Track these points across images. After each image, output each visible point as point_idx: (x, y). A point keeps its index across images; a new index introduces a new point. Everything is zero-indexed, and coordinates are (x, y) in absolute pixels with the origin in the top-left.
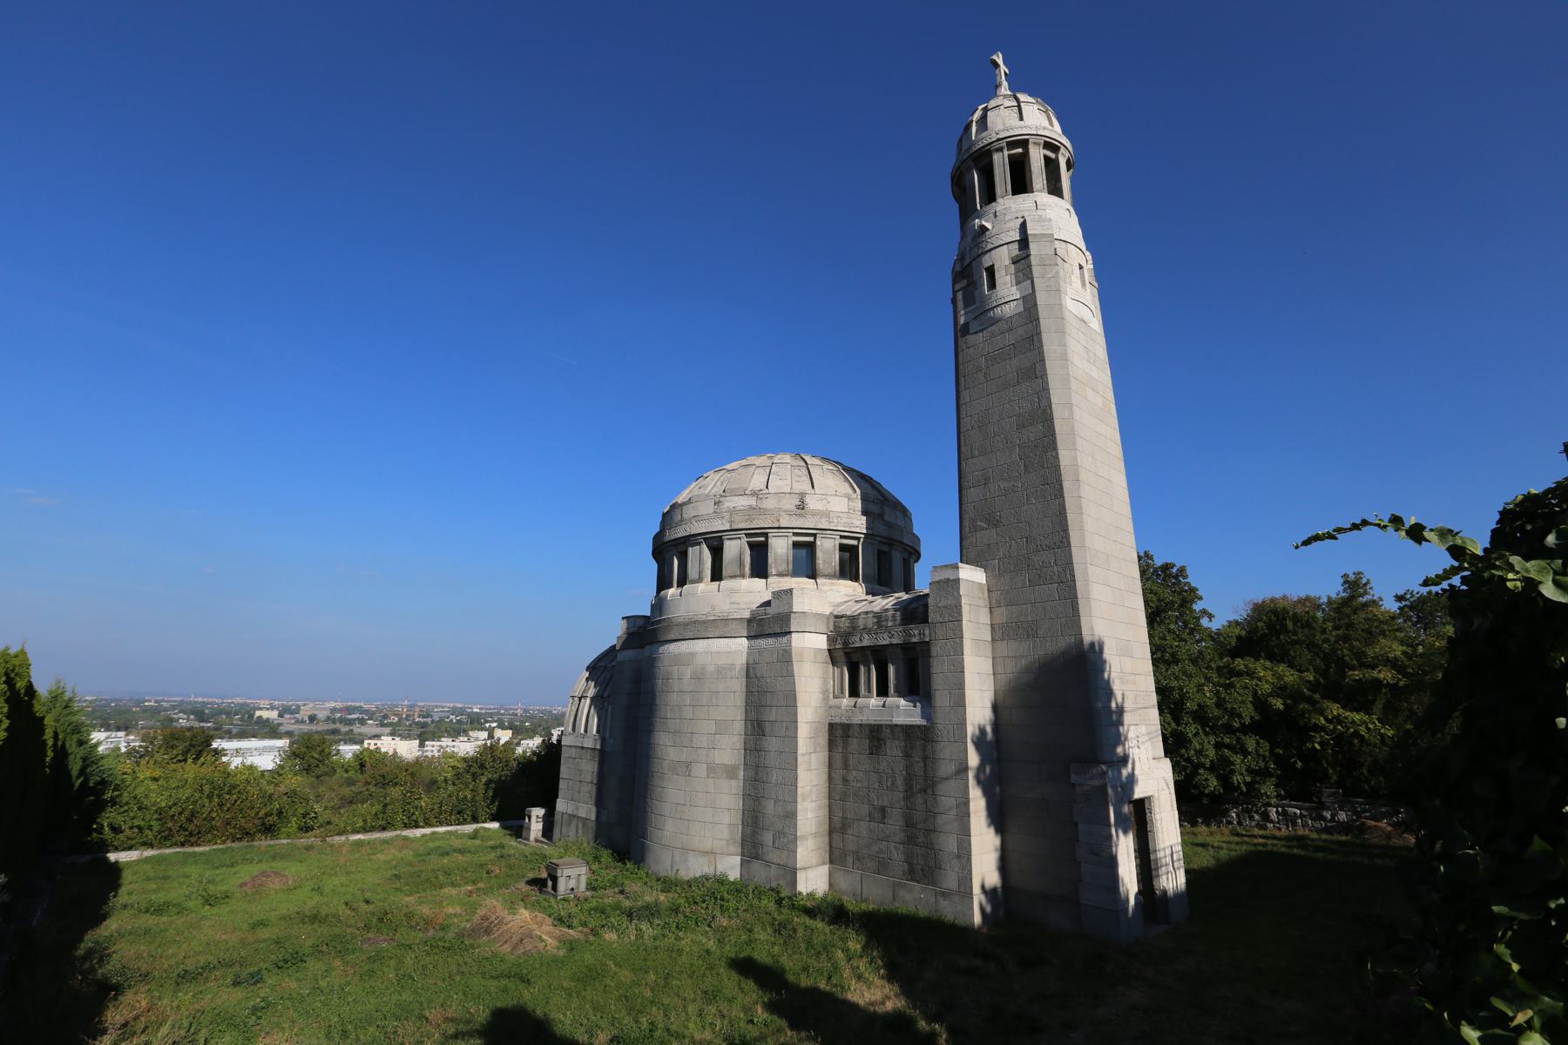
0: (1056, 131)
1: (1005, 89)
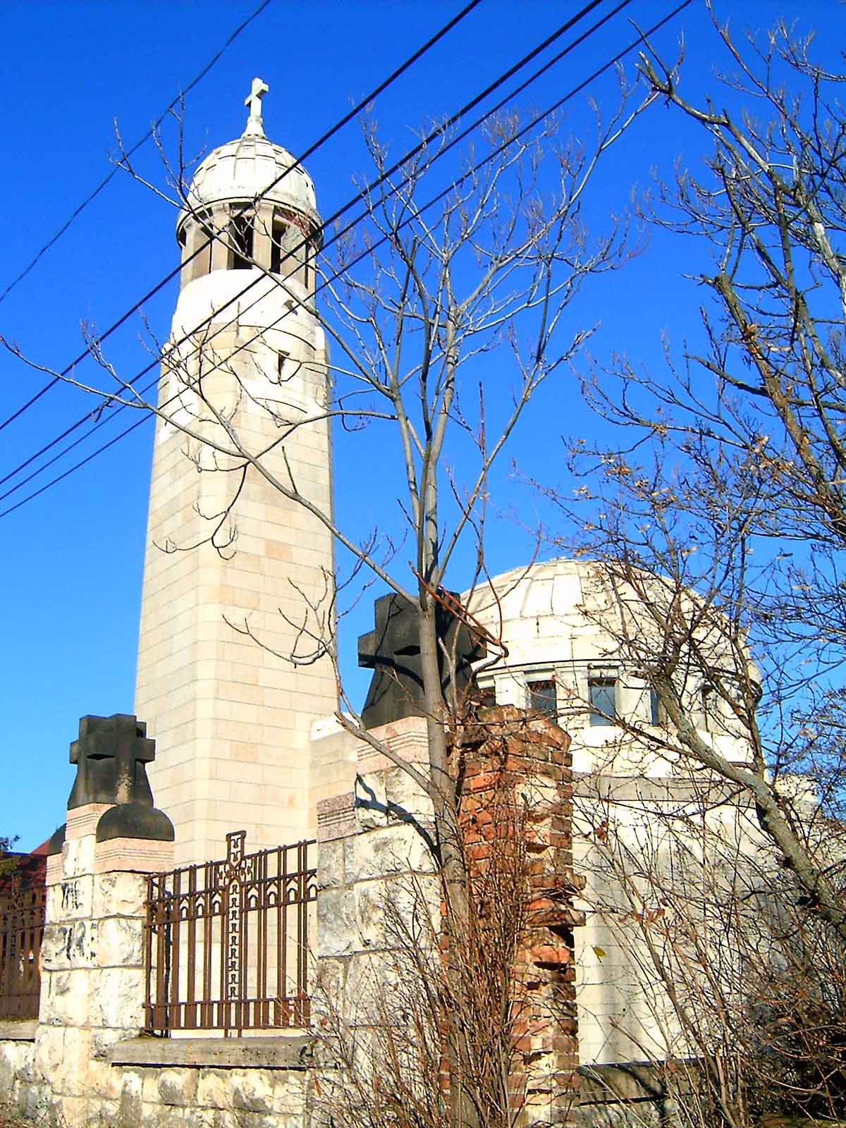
0: (299, 190)
1: (254, 126)
